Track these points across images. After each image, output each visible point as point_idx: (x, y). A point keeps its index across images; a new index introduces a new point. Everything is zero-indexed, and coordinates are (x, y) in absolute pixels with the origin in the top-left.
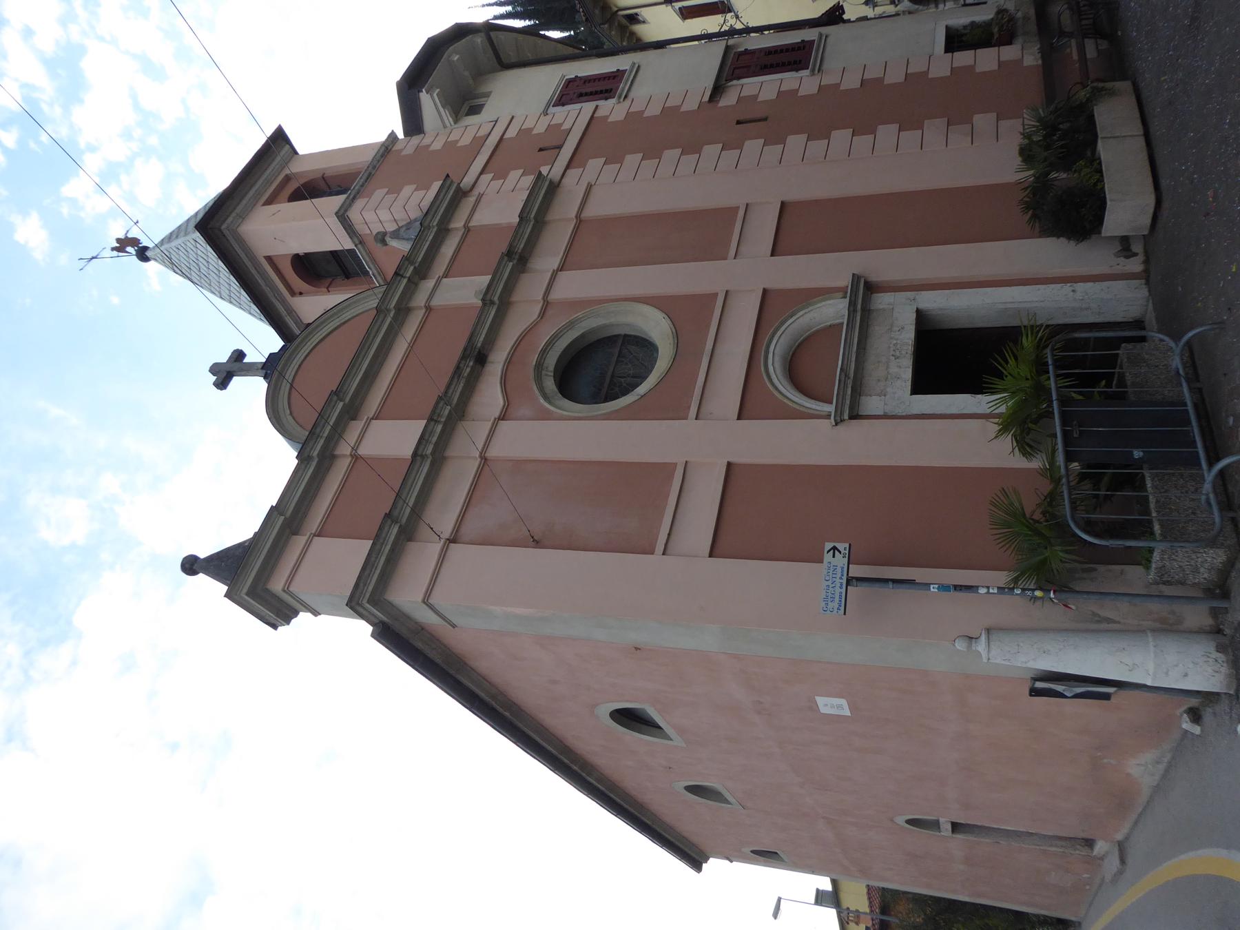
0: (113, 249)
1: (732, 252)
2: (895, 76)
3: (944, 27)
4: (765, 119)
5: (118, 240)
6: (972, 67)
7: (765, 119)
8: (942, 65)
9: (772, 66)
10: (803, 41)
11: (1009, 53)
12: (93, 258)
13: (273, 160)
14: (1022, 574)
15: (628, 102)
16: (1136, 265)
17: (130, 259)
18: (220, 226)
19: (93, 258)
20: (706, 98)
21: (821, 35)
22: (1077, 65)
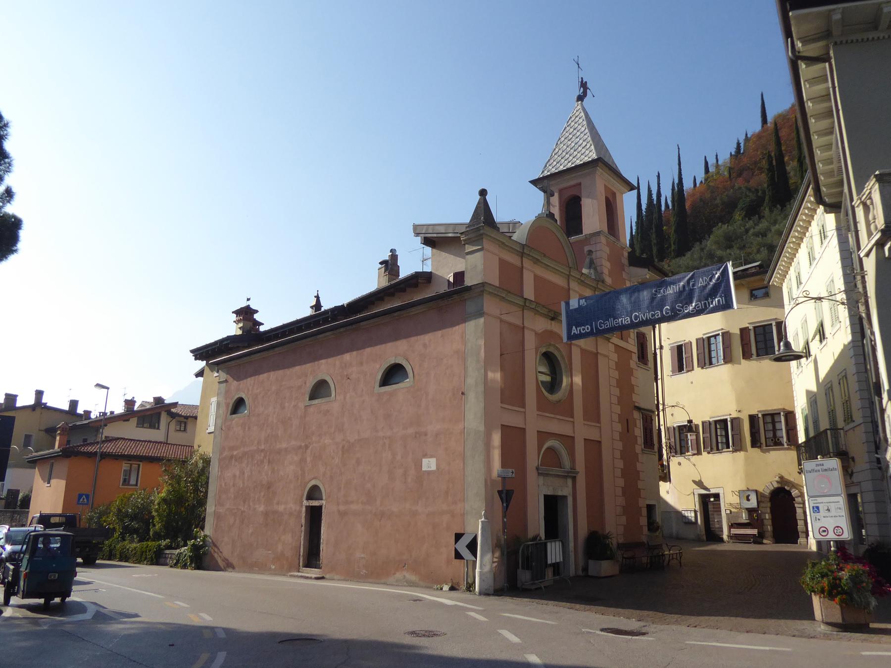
0: (582, 78)
1: (585, 423)
2: (640, 485)
3: (655, 504)
4: (628, 431)
5: (586, 82)
6: (641, 516)
7: (628, 431)
8: (643, 503)
9: (646, 437)
10: (654, 445)
11: (645, 529)
12: (578, 64)
13: (623, 186)
14: (493, 552)
15: (636, 368)
16: (580, 573)
17: (578, 91)
18: (599, 167)
19: (578, 64)
20: (637, 404)
21: (656, 452)
22: (625, 287)
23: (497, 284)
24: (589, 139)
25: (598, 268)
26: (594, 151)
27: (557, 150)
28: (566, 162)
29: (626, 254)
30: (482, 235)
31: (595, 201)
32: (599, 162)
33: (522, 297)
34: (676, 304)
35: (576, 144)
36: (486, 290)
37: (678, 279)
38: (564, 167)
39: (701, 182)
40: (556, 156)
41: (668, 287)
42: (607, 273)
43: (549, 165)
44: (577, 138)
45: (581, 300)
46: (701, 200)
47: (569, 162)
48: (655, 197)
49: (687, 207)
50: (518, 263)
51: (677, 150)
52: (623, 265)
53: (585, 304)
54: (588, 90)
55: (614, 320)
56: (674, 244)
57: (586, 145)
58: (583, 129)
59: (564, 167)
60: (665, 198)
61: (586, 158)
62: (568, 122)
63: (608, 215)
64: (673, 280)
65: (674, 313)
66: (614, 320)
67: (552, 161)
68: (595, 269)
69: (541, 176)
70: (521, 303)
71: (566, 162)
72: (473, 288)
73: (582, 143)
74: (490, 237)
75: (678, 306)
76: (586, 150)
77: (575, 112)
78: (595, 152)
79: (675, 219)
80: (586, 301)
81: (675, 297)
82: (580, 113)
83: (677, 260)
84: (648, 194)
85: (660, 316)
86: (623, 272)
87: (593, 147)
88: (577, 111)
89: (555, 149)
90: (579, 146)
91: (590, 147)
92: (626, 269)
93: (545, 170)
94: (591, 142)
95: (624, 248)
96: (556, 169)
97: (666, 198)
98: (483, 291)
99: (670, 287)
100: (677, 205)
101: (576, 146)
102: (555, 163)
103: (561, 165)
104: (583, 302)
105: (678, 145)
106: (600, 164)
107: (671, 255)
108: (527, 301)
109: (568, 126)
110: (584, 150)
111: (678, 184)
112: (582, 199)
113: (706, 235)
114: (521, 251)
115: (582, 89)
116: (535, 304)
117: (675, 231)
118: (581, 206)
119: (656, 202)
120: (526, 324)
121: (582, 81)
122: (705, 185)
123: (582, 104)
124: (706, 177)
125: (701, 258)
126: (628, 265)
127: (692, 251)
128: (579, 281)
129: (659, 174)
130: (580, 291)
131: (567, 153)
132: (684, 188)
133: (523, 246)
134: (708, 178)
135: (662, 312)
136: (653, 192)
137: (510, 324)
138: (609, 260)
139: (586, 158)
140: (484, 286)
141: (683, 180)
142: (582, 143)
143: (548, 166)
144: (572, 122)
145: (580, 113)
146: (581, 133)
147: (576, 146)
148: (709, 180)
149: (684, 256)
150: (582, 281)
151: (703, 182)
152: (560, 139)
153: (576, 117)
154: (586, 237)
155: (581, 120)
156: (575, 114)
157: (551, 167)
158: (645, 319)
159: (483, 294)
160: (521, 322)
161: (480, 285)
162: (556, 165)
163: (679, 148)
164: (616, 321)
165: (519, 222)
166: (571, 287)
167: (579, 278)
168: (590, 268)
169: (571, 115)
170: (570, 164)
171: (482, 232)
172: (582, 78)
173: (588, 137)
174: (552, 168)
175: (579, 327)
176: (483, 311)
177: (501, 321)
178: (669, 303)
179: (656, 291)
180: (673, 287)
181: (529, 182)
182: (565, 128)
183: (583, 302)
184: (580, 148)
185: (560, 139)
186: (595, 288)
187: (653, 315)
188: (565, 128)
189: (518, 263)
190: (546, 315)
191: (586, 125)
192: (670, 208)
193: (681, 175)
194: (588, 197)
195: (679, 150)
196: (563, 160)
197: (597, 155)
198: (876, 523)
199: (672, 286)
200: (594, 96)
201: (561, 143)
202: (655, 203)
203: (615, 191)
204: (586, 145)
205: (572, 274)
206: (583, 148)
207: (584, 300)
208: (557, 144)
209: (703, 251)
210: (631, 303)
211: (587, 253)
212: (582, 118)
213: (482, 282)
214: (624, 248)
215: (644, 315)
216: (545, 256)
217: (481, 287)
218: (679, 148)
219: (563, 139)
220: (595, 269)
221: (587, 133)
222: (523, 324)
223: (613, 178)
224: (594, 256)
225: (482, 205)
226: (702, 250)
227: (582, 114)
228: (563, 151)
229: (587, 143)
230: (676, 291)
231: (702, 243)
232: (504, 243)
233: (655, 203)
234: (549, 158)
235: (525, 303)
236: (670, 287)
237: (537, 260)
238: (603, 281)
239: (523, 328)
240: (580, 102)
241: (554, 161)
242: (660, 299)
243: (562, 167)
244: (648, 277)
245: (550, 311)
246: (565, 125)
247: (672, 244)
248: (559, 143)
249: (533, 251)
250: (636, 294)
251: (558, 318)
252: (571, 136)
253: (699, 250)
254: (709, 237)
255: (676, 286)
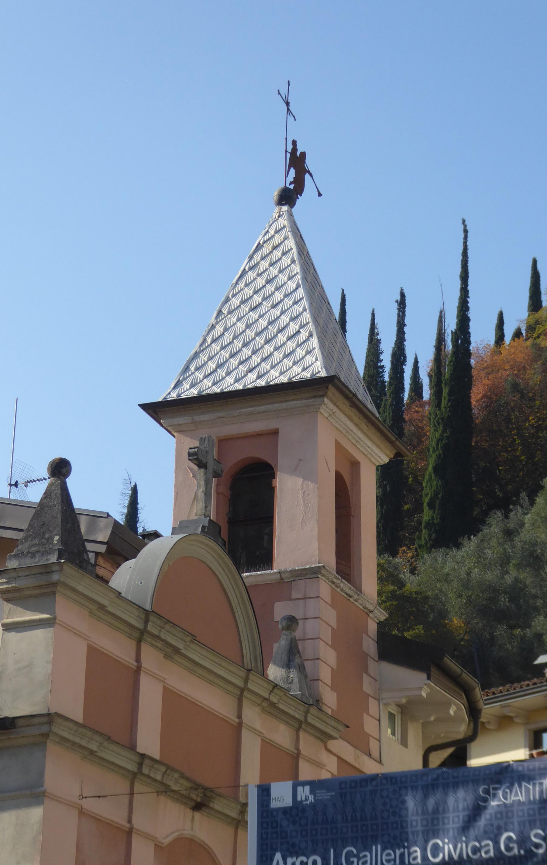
0: (294, 143)
5: (303, 154)
12: (288, 104)
19: (288, 104)
23: (79, 717)
24: (307, 316)
25: (308, 665)
26: (317, 352)
27: (219, 329)
28: (243, 368)
29: (373, 627)
30: (54, 584)
31: (311, 485)
32: (330, 386)
33: (132, 748)
34: (532, 829)
35: (270, 323)
36: (56, 734)
37: (540, 769)
38: (237, 381)
39: (518, 334)
40: (216, 347)
41: (516, 785)
42: (328, 680)
43: (197, 369)
44: (274, 306)
45: (300, 789)
46: (515, 387)
47: (251, 370)
48: (386, 360)
49: (473, 402)
50: (130, 660)
51: (462, 235)
52: (365, 656)
53: (311, 798)
54: (307, 176)
55: (383, 850)
56: (431, 505)
57: (298, 332)
58: (292, 285)
59: (237, 381)
60: (413, 360)
61: (297, 369)
62: (251, 257)
63: (338, 517)
64: (529, 770)
65: (526, 851)
66: (383, 850)
67: (203, 358)
68: (301, 669)
69: (174, 396)
70: (133, 767)
71: (243, 368)
72: (20, 723)
73: (288, 325)
74: (74, 590)
75: (536, 836)
76: (299, 345)
77: (272, 232)
78: (320, 357)
79: (438, 435)
80: (312, 792)
81: (531, 812)
82: (286, 238)
83: (439, 554)
84: (369, 350)
85: (492, 854)
86: (365, 676)
87: (314, 342)
88: (277, 232)
89: (213, 327)
90: (280, 331)
91: (307, 340)
92: (372, 666)
93: (184, 379)
94: (311, 326)
95: (371, 612)
96: (214, 384)
97: (416, 362)
98: (46, 736)
99: (520, 787)
100: (450, 394)
101: (273, 330)
102: (212, 365)
103: (228, 374)
104: (304, 793)
105: (464, 221)
106: (332, 390)
107: (419, 538)
108: (147, 761)
109: (251, 269)
110: (291, 345)
111: (456, 336)
112: (279, 475)
113: (523, 494)
114: (140, 626)
115: (292, 171)
116: (163, 769)
117: (435, 469)
118: (271, 490)
119: (391, 378)
120: (138, 822)
121: (295, 150)
122: (529, 343)
123: (291, 215)
124: (532, 322)
125: (505, 561)
126: (376, 658)
127: (480, 535)
128: (265, 704)
129: (403, 295)
130: (264, 732)
131: (245, 345)
132: (473, 347)
133: (147, 615)
134: (537, 322)
135: (496, 843)
136: (382, 346)
137: (98, 820)
138: (333, 646)
139: (297, 369)
140: (50, 723)
141: (471, 324)
142: (288, 325)
143: (192, 368)
144: (263, 258)
145: (286, 238)
146: (286, 296)
147: (273, 330)
148: (540, 329)
149: (458, 546)
150: (272, 705)
151: (524, 332)
152: (227, 300)
153: (275, 248)
154: (282, 579)
155: (286, 261)
156: (272, 237)
157: (199, 375)
158: (456, 857)
159: (45, 744)
160: (125, 814)
161: (40, 720)
162: (215, 371)
163: (466, 232)
164: (389, 854)
165: (108, 515)
166: (245, 719)
167: (267, 697)
168: (288, 665)
169: (260, 239)
170: (252, 376)
171: (55, 577)
172: (294, 143)
173: (304, 310)
174: (206, 377)
175: (291, 855)
176: (42, 789)
177: (82, 812)
178: (516, 824)
179: (487, 792)
180: (526, 786)
181: (140, 405)
182: (244, 273)
183: (304, 793)
184: (281, 338)
185: (227, 300)
186: (300, 723)
187: (476, 850)
188: (244, 273)
189: (130, 660)
190: (183, 796)
191: (299, 276)
192: (427, 394)
193: (467, 309)
194: (294, 471)
195: (466, 237)
196: (234, 362)
197: (326, 367)
198: (323, 770)
199: (524, 784)
200: (320, 195)
201: (230, 312)
202: (387, 378)
203: (358, 457)
204: (298, 332)
205: (250, 686)
206: (290, 338)
207: (307, 788)
208: (220, 312)
209: (512, 540)
210: (424, 812)
211: (284, 623)
212: (290, 255)
213: (45, 711)
214: (371, 612)
215: (455, 848)
216: (194, 638)
217: (43, 724)
218: (466, 232)
219: (235, 302)
220: (301, 669)
221: (301, 299)
222: (130, 821)
223: (356, 425)
224: (298, 634)
225: (57, 502)
226: (509, 534)
227: (291, 243)
228: (235, 337)
229: (302, 327)
230: (534, 798)
231: (512, 515)
232: (105, 606)
233: (387, 378)
234: (196, 348)
235: (140, 765)
236: (520, 787)
237: (177, 650)
238: (318, 703)
239: (129, 832)
240: (285, 208)
241: (210, 358)
242: (496, 813)
243: (230, 380)
244: (424, 694)
245: (196, 786)
246: (244, 264)
247: (425, 505)
248: (225, 311)
249: (167, 627)
250: (439, 794)
251: (211, 805)
252: (257, 299)
253: (500, 535)
254: (532, 502)
255: (534, 785)
